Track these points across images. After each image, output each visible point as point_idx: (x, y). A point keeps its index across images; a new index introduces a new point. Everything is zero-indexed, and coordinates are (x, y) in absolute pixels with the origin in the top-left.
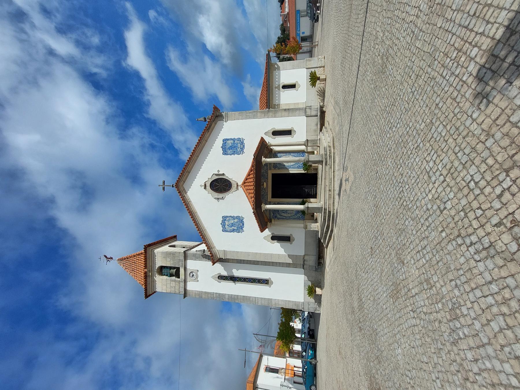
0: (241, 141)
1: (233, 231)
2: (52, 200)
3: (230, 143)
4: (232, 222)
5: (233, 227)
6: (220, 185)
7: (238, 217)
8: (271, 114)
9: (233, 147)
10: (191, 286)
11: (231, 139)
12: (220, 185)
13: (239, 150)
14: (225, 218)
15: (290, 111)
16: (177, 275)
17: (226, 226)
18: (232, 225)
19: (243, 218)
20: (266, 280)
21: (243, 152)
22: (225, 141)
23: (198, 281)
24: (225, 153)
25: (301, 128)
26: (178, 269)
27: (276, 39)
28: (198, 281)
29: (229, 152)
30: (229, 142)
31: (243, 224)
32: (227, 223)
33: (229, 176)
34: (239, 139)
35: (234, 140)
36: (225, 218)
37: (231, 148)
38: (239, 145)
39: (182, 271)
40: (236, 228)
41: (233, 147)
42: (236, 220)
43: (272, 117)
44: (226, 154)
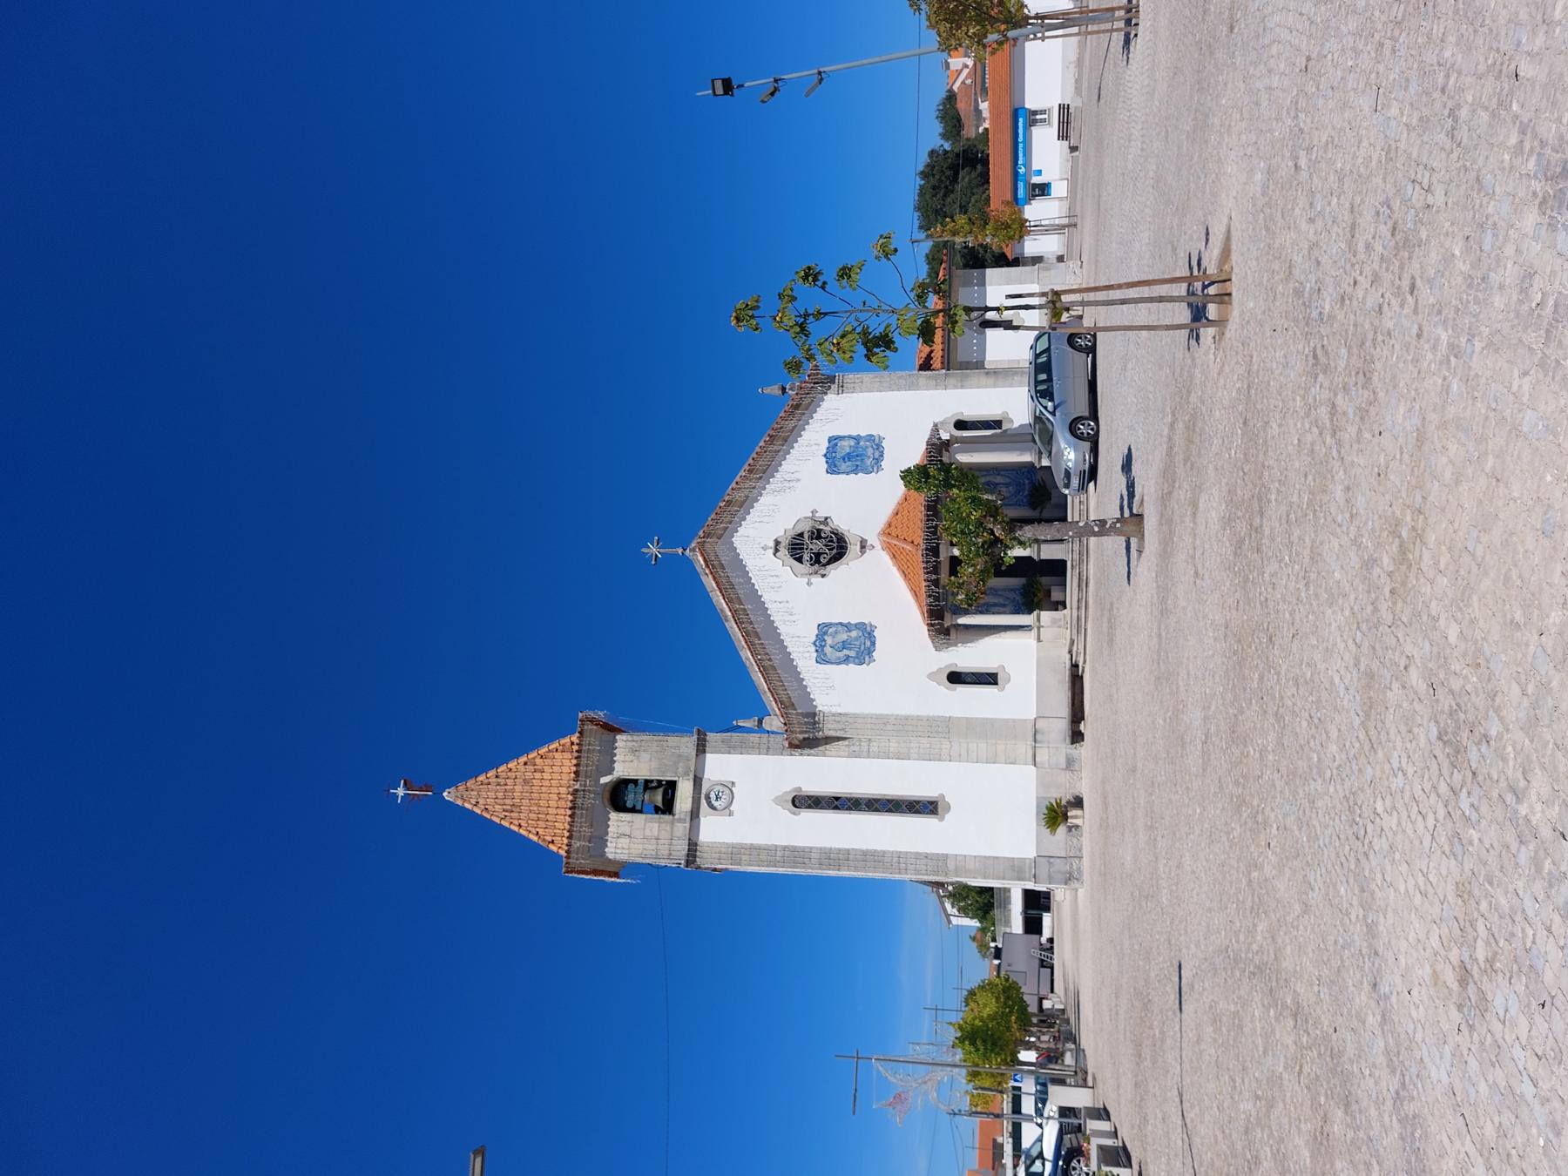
0: (876, 443)
1: (847, 660)
2: (907, 475)
3: (846, 446)
4: (844, 637)
5: (846, 652)
6: (820, 547)
7: (861, 626)
8: (952, 381)
9: (852, 456)
10: (713, 830)
11: (850, 437)
12: (820, 547)
13: (869, 462)
14: (824, 629)
15: (1003, 374)
16: (667, 807)
17: (828, 649)
18: (845, 645)
19: (873, 628)
20: (931, 803)
21: (879, 469)
22: (834, 441)
23: (731, 814)
24: (833, 467)
25: (1014, 404)
26: (671, 786)
27: (923, 159)
28: (731, 814)
29: (843, 466)
30: (845, 443)
31: (873, 644)
32: (829, 640)
33: (843, 522)
34: (870, 438)
35: (857, 439)
36: (824, 629)
37: (848, 457)
38: (870, 451)
39: (684, 791)
40: (852, 654)
41: (852, 456)
42: (854, 634)
43: (955, 387)
44: (834, 472)
